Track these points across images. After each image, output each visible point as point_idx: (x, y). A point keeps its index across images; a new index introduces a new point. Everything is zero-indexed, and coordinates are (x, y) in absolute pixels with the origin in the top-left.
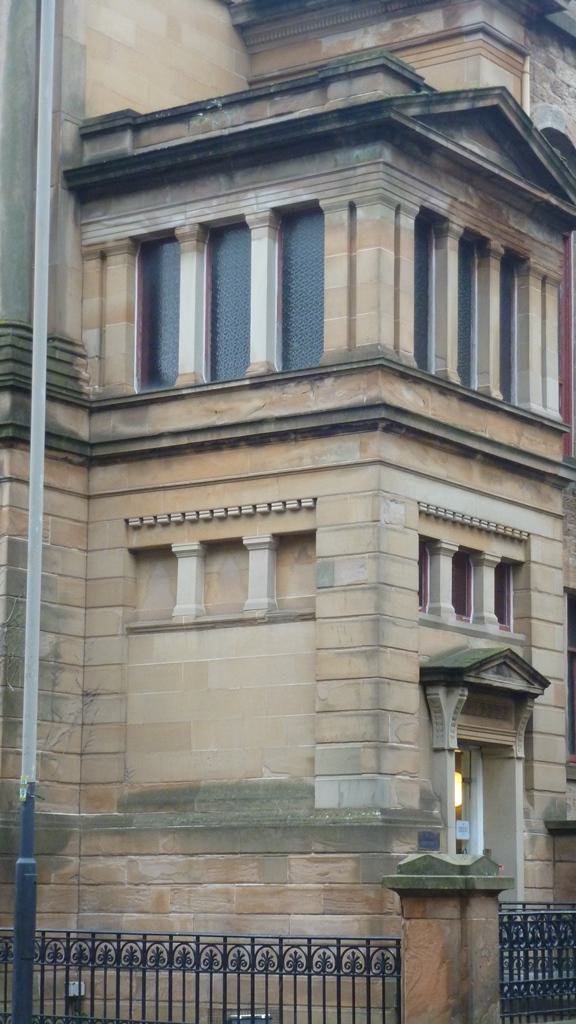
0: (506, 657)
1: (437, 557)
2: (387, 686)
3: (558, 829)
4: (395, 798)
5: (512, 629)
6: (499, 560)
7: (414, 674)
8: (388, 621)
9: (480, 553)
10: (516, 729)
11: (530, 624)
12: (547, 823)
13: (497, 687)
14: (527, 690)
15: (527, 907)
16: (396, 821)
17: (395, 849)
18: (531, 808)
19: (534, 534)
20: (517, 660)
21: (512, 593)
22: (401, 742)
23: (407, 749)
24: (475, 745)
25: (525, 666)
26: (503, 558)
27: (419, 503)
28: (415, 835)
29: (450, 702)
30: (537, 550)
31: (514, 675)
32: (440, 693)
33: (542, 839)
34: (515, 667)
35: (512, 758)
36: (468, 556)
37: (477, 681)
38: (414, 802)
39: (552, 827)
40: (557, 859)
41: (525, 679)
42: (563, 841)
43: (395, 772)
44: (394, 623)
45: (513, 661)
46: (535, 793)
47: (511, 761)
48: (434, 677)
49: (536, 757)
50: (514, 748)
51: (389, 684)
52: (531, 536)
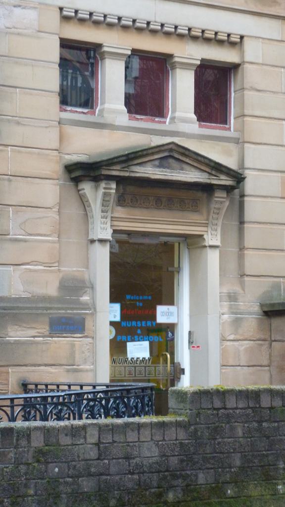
0: (171, 150)
1: (104, 60)
2: (6, 183)
3: (274, 312)
4: (21, 288)
5: (232, 129)
6: (199, 63)
7: (54, 168)
8: (9, 121)
9: (100, 46)
10: (207, 220)
11: (243, 121)
12: (262, 305)
13: (154, 179)
14: (208, 181)
15: (97, 387)
16: (18, 308)
17: (11, 334)
18: (241, 292)
19: (248, 36)
20: (187, 153)
21: (233, 94)
22: (31, 235)
23: (36, 241)
24: (125, 234)
25: (200, 158)
26: (202, 60)
27: (61, 9)
28: (47, 320)
29: (95, 194)
30: (252, 51)
31: (185, 166)
32: (87, 187)
33: (251, 324)
34: (187, 160)
35: (205, 247)
36: (165, 60)
37: (127, 174)
38: (52, 290)
39: (266, 309)
40: (273, 339)
41: (206, 171)
42: (277, 322)
43: (20, 263)
44: (18, 123)
45: (183, 154)
46: (246, 279)
47: (205, 250)
48: (81, 172)
49: (247, 244)
50: (205, 237)
51: (10, 180)
52: (245, 39)
